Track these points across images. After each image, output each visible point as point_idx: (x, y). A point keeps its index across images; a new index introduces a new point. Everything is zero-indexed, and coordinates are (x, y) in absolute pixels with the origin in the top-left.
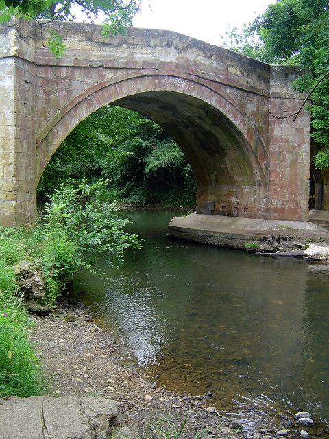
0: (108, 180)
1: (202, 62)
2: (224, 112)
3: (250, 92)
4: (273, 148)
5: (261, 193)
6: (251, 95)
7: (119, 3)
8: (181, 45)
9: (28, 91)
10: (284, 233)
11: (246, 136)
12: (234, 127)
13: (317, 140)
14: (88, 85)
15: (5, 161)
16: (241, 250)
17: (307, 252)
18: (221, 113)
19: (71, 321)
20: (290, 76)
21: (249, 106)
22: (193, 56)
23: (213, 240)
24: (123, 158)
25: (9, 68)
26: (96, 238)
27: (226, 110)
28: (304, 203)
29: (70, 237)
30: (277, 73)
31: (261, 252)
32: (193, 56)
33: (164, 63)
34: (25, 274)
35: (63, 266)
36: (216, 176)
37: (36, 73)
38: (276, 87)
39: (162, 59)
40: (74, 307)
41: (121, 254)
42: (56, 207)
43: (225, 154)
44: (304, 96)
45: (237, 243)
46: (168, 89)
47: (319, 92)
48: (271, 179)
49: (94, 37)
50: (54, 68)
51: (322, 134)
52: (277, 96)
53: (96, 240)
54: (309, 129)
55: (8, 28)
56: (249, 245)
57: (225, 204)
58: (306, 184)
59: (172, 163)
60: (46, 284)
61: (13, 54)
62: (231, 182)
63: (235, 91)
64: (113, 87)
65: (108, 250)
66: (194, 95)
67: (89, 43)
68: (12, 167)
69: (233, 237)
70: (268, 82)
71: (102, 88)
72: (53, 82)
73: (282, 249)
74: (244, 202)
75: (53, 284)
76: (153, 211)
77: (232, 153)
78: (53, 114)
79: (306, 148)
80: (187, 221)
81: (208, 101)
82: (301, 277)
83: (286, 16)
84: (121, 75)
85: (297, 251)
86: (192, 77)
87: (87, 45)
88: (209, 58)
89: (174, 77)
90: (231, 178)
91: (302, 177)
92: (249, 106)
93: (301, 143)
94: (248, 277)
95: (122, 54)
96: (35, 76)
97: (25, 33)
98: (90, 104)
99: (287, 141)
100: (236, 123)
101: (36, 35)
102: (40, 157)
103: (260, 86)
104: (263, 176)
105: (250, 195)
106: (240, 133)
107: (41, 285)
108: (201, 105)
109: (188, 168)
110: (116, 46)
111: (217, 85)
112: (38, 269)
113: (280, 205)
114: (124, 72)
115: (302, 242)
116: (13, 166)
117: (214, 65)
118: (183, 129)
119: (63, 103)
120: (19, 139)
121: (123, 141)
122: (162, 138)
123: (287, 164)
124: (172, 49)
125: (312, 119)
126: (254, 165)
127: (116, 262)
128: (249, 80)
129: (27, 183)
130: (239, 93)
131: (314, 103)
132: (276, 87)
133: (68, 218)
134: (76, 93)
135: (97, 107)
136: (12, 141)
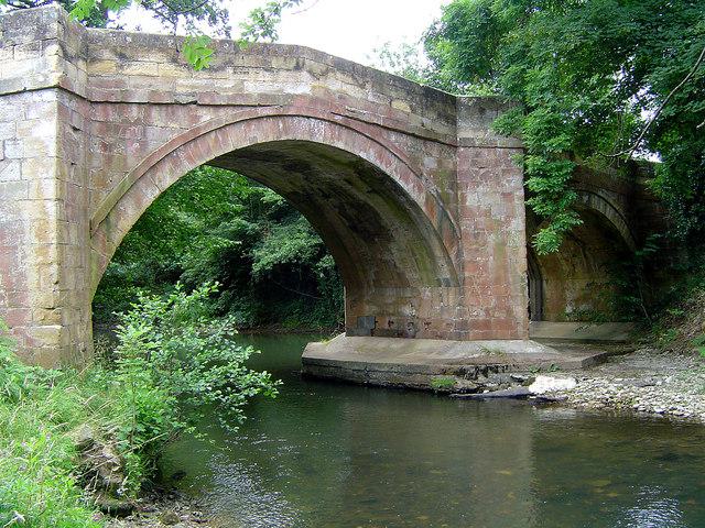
0: (217, 283)
1: (352, 94)
2: (388, 173)
3: (427, 139)
4: (466, 225)
5: (451, 298)
6: (429, 144)
7: (210, 4)
8: (318, 67)
9: (77, 144)
10: (493, 360)
11: (424, 209)
12: (404, 194)
13: (537, 210)
14: (173, 132)
15: (41, 258)
16: (425, 392)
17: (532, 388)
18: (384, 173)
19: (171, 523)
20: (488, 112)
21: (427, 160)
22: (337, 84)
23: (375, 378)
24: (216, 253)
25: (47, 107)
26: (202, 382)
27: (392, 169)
28: (520, 311)
29: (156, 382)
30: (468, 108)
31: (459, 392)
32: (337, 84)
33: (292, 97)
34: (86, 447)
35: (148, 430)
36: (376, 273)
37: (92, 114)
38: (467, 130)
39: (289, 90)
40: (169, 498)
41: (240, 407)
42: (131, 332)
43: (390, 239)
44: (511, 142)
45: (418, 380)
46: (299, 137)
47: (537, 134)
48: (467, 274)
49: (181, 56)
50: (117, 106)
51: (544, 201)
52: (468, 143)
53: (201, 385)
54: (522, 193)
55: (46, 42)
56: (438, 382)
57: (393, 318)
58: (523, 280)
59: (296, 257)
60: (123, 461)
61: (53, 82)
62: (402, 282)
63: (404, 139)
64: (213, 135)
65: (219, 401)
66: (341, 145)
67: (173, 66)
68: (54, 269)
69: (411, 370)
70: (454, 123)
71: (196, 137)
72: (117, 129)
73: (492, 386)
74: (424, 314)
75: (135, 462)
76: (266, 336)
77: (401, 236)
78: (117, 180)
79: (518, 224)
80: (332, 348)
81: (363, 155)
82: (522, 431)
83: (479, 19)
84: (226, 116)
85: (516, 389)
86: (337, 118)
87: (170, 69)
88: (362, 86)
89: (308, 117)
90: (400, 276)
91: (515, 268)
92: (427, 160)
93: (510, 216)
94: (438, 434)
95: (227, 83)
96: (88, 120)
97: (72, 50)
98: (176, 164)
99: (488, 213)
100: (408, 187)
101: (88, 55)
102: (98, 251)
103: (441, 129)
104: (453, 272)
105: (433, 302)
106: (414, 204)
107: (115, 465)
108: (351, 162)
109: (327, 261)
110: (216, 71)
111: (378, 129)
112: (107, 437)
113: (482, 316)
114: (230, 111)
115: (523, 373)
116: (55, 266)
117: (370, 98)
118: (320, 201)
119: (133, 163)
120: (63, 222)
121: (216, 224)
122: (280, 215)
123: (490, 249)
124: (304, 75)
125: (527, 177)
126: (438, 253)
127: (232, 420)
128: (424, 120)
129: (78, 294)
130: (410, 141)
131: (529, 151)
132: (467, 130)
133: (154, 349)
134: (153, 146)
135: (187, 167)
136: (53, 225)
